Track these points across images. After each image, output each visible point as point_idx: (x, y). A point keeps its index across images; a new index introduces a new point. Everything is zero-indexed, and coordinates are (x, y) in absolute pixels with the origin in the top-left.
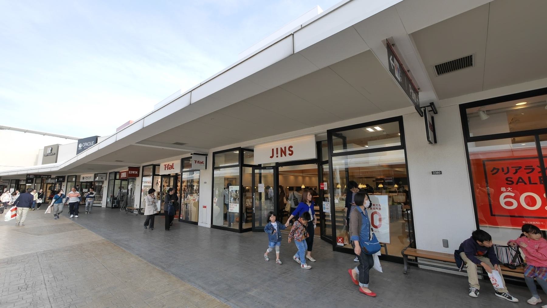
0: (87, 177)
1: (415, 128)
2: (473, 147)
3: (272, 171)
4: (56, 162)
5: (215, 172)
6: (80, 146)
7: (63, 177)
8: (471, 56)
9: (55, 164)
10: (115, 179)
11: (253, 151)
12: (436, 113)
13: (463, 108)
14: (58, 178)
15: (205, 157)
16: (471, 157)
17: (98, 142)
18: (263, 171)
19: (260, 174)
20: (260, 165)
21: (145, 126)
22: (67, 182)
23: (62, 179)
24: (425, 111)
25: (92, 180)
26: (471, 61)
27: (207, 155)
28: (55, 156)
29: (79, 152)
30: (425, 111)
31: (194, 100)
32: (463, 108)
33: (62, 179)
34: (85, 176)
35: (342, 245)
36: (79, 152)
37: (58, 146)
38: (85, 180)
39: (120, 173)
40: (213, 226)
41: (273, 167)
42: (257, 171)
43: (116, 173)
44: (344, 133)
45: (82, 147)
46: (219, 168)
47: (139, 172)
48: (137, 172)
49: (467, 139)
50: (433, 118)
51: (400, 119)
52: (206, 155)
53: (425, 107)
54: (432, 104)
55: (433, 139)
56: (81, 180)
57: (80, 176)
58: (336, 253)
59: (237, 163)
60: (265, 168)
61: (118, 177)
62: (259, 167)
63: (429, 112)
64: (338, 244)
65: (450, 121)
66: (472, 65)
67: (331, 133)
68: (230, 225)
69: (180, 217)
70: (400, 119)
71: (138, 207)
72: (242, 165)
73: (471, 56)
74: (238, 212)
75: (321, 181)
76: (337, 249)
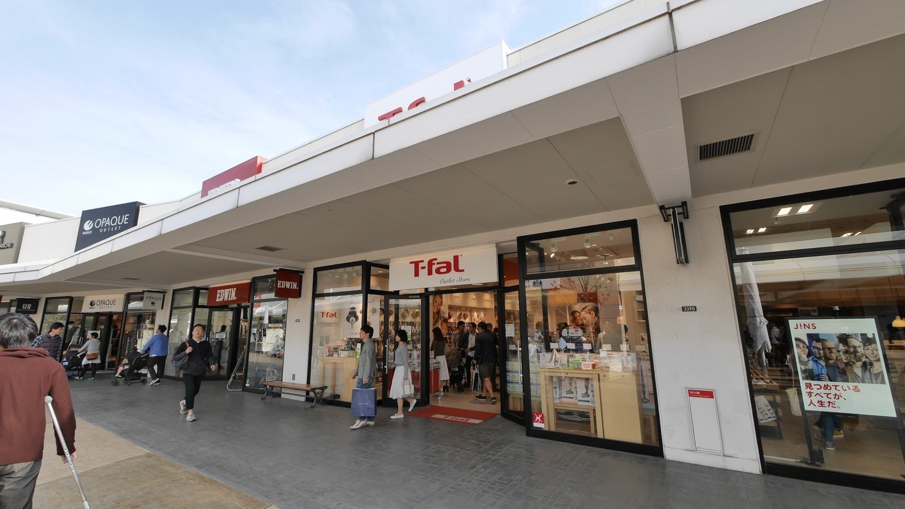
0: (103, 302)
1: (657, 239)
2: (756, 274)
3: (418, 302)
4: (16, 261)
5: (318, 302)
6: (88, 226)
7: (35, 303)
8: (752, 135)
9: (15, 265)
10: (196, 305)
11: (387, 267)
12: (687, 217)
13: (726, 211)
14: (20, 302)
15: (161, 295)
16: (315, 310)
17: (141, 221)
18: (402, 302)
19: (397, 307)
20: (397, 292)
21: (241, 203)
22: (45, 312)
23: (29, 306)
24: (674, 212)
25: (118, 308)
26: (750, 144)
27: (303, 272)
28: (12, 251)
29: (83, 241)
30: (674, 212)
31: (17, 279)
32: (726, 211)
33: (29, 306)
34: (96, 298)
35: (542, 426)
36: (83, 241)
37: (21, 228)
38: (96, 309)
39: (213, 292)
40: (769, 468)
41: (420, 296)
42: (392, 302)
43: (197, 291)
44: (542, 243)
45: (93, 229)
46: (323, 295)
47: (300, 285)
48: (295, 286)
49: (734, 258)
50: (681, 224)
51: (632, 224)
52: (164, 292)
53: (673, 208)
54: (684, 204)
55: (683, 258)
56: (86, 309)
57: (81, 300)
58: (772, 478)
59: (359, 288)
60: (406, 296)
61: (202, 301)
62: (396, 294)
63: (676, 215)
64: (535, 425)
65: (707, 230)
66: (749, 149)
67: (523, 242)
68: (816, 456)
69: (245, 383)
70: (632, 224)
71: (301, 380)
72: (367, 291)
73: (701, 159)
74: (448, 378)
75: (502, 322)
76: (245, 389)
